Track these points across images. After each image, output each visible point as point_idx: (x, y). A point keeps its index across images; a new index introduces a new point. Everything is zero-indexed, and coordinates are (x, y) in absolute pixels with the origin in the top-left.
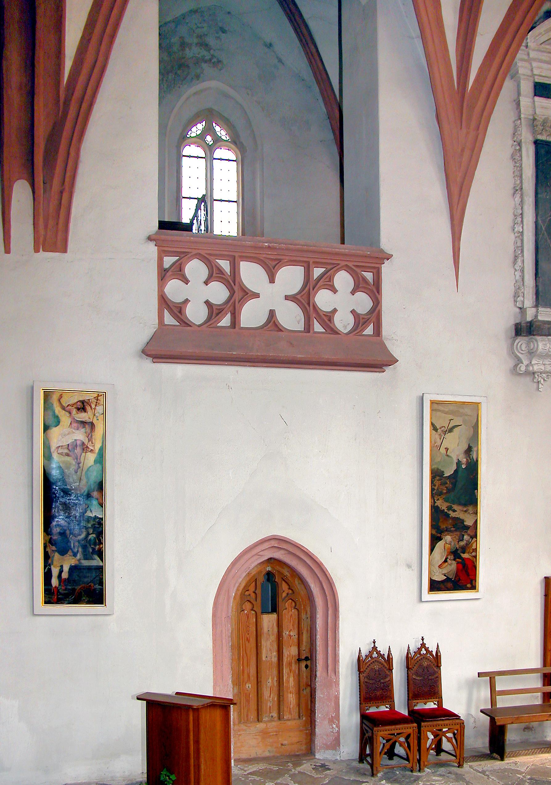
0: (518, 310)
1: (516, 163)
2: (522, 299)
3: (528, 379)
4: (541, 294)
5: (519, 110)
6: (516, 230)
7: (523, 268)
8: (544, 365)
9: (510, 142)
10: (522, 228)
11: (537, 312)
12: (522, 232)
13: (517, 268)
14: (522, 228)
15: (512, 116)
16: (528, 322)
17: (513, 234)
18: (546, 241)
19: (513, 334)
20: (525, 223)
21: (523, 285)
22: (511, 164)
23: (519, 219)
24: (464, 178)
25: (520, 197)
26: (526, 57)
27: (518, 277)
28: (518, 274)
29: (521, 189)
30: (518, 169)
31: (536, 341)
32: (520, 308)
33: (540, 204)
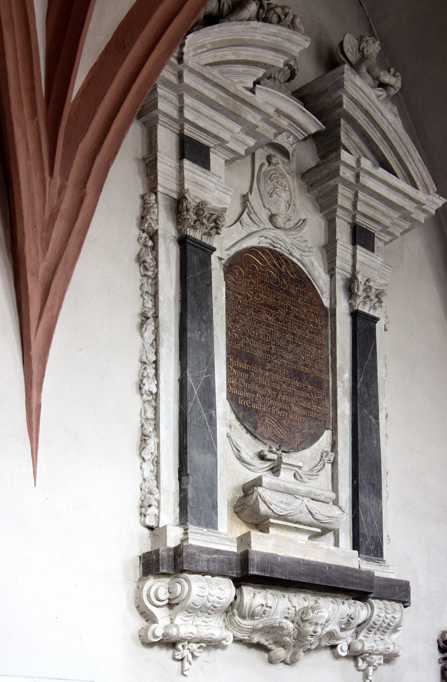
0: (147, 532)
1: (146, 269)
2: (156, 511)
3: (165, 654)
4: (190, 504)
5: (152, 177)
6: (146, 388)
7: (158, 457)
8: (197, 626)
9: (136, 232)
10: (157, 386)
11: (186, 534)
12: (157, 394)
13: (146, 457)
14: (157, 386)
15: (138, 186)
16: (169, 549)
17: (139, 396)
18: (200, 414)
19: (137, 572)
20: (162, 378)
21: (158, 487)
22: (135, 270)
23: (151, 371)
24: (54, 273)
25: (153, 331)
26: (174, 79)
27: (147, 474)
28: (148, 467)
29: (156, 317)
30: (150, 281)
31: (187, 580)
32: (151, 528)
33: (190, 350)
